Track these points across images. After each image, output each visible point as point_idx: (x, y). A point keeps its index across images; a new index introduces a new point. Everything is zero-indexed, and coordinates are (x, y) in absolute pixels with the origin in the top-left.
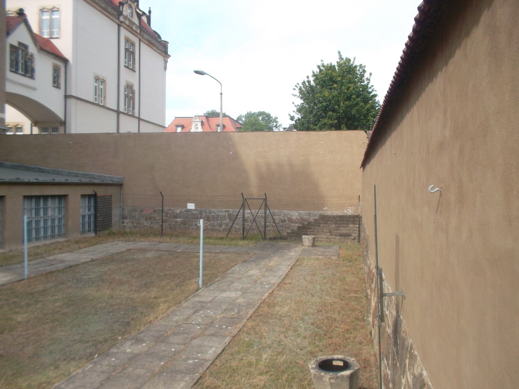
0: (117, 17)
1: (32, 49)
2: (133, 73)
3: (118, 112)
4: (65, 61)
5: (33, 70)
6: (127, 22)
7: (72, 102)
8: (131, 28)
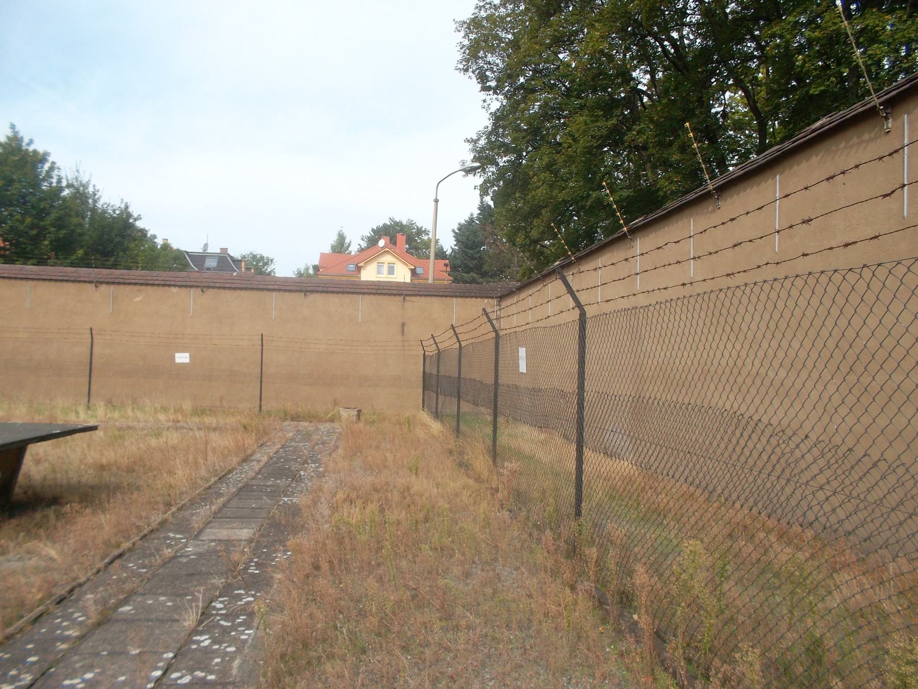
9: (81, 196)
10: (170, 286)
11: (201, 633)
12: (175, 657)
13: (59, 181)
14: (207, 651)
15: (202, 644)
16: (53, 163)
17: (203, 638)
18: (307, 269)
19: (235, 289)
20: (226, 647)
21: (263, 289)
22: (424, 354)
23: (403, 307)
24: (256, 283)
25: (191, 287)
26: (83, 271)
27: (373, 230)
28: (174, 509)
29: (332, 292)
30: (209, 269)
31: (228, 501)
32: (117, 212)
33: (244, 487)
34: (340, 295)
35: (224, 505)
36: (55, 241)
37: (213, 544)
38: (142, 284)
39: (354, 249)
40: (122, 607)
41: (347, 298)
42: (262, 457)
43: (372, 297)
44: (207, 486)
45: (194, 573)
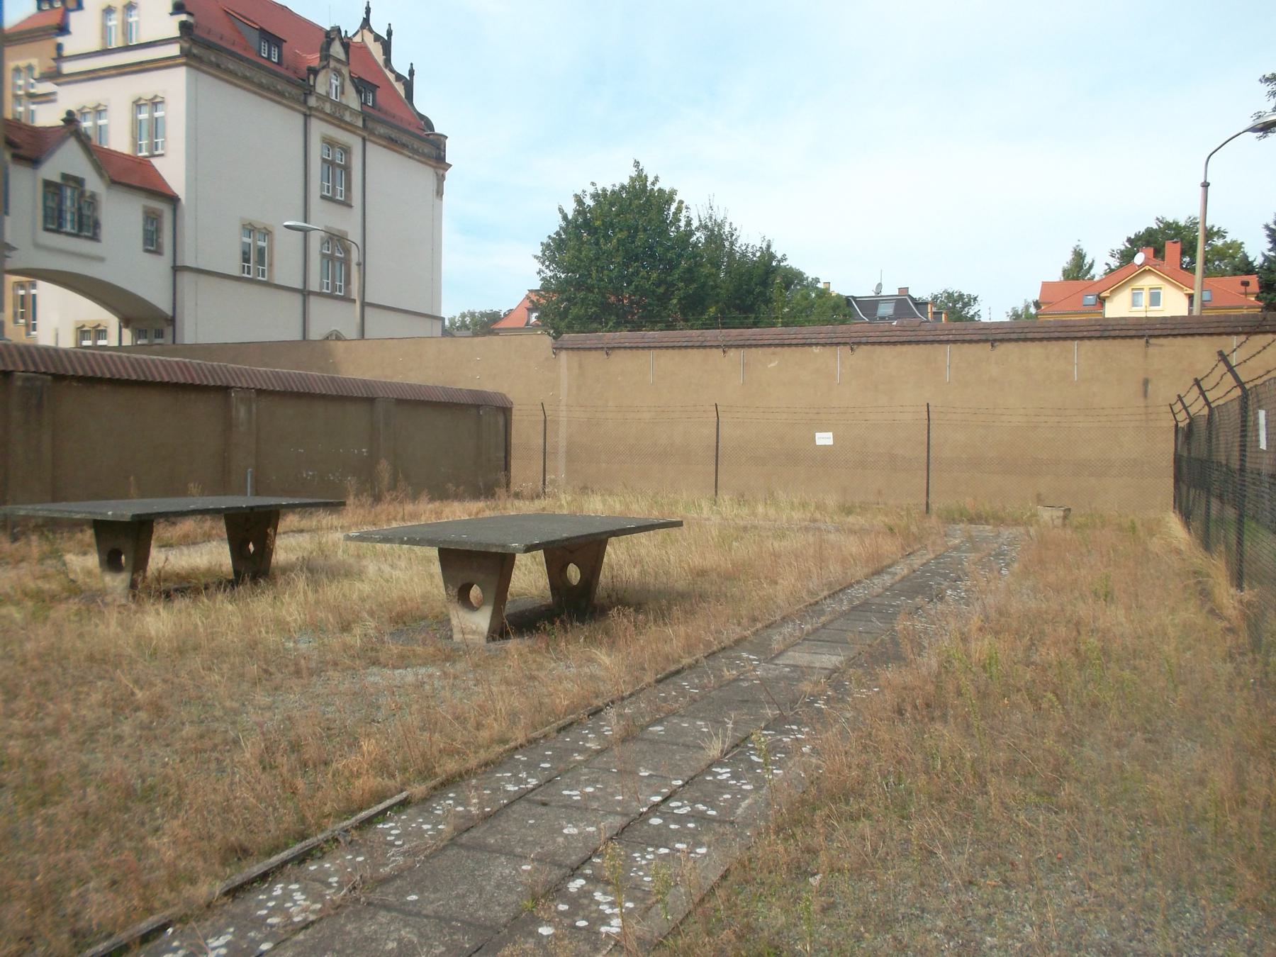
0: (302, 98)
1: (94, 184)
2: (345, 209)
3: (305, 293)
4: (173, 200)
5: (96, 225)
6: (328, 108)
7: (186, 279)
8: (341, 120)
9: (717, 237)
10: (810, 345)
11: (722, 765)
12: (683, 786)
13: (689, 223)
14: (722, 786)
15: (719, 777)
16: (681, 202)
17: (724, 770)
18: (1027, 307)
19: (895, 343)
20: (744, 784)
21: (932, 342)
22: (1177, 426)
23: (1146, 355)
24: (923, 333)
25: (838, 344)
26: (710, 334)
27: (1129, 240)
28: (759, 625)
29: (1033, 340)
30: (882, 318)
31: (831, 621)
32: (758, 254)
33: (860, 605)
34: (1045, 343)
35: (824, 626)
36: (684, 298)
37: (788, 669)
38: (777, 345)
39: (1098, 271)
40: (654, 726)
41: (1055, 347)
42: (901, 570)
43: (1095, 342)
44: (812, 601)
45: (748, 701)
